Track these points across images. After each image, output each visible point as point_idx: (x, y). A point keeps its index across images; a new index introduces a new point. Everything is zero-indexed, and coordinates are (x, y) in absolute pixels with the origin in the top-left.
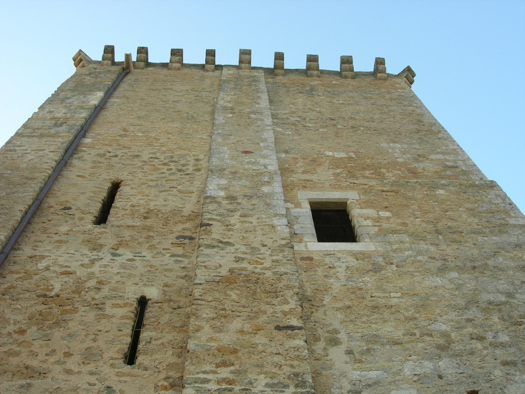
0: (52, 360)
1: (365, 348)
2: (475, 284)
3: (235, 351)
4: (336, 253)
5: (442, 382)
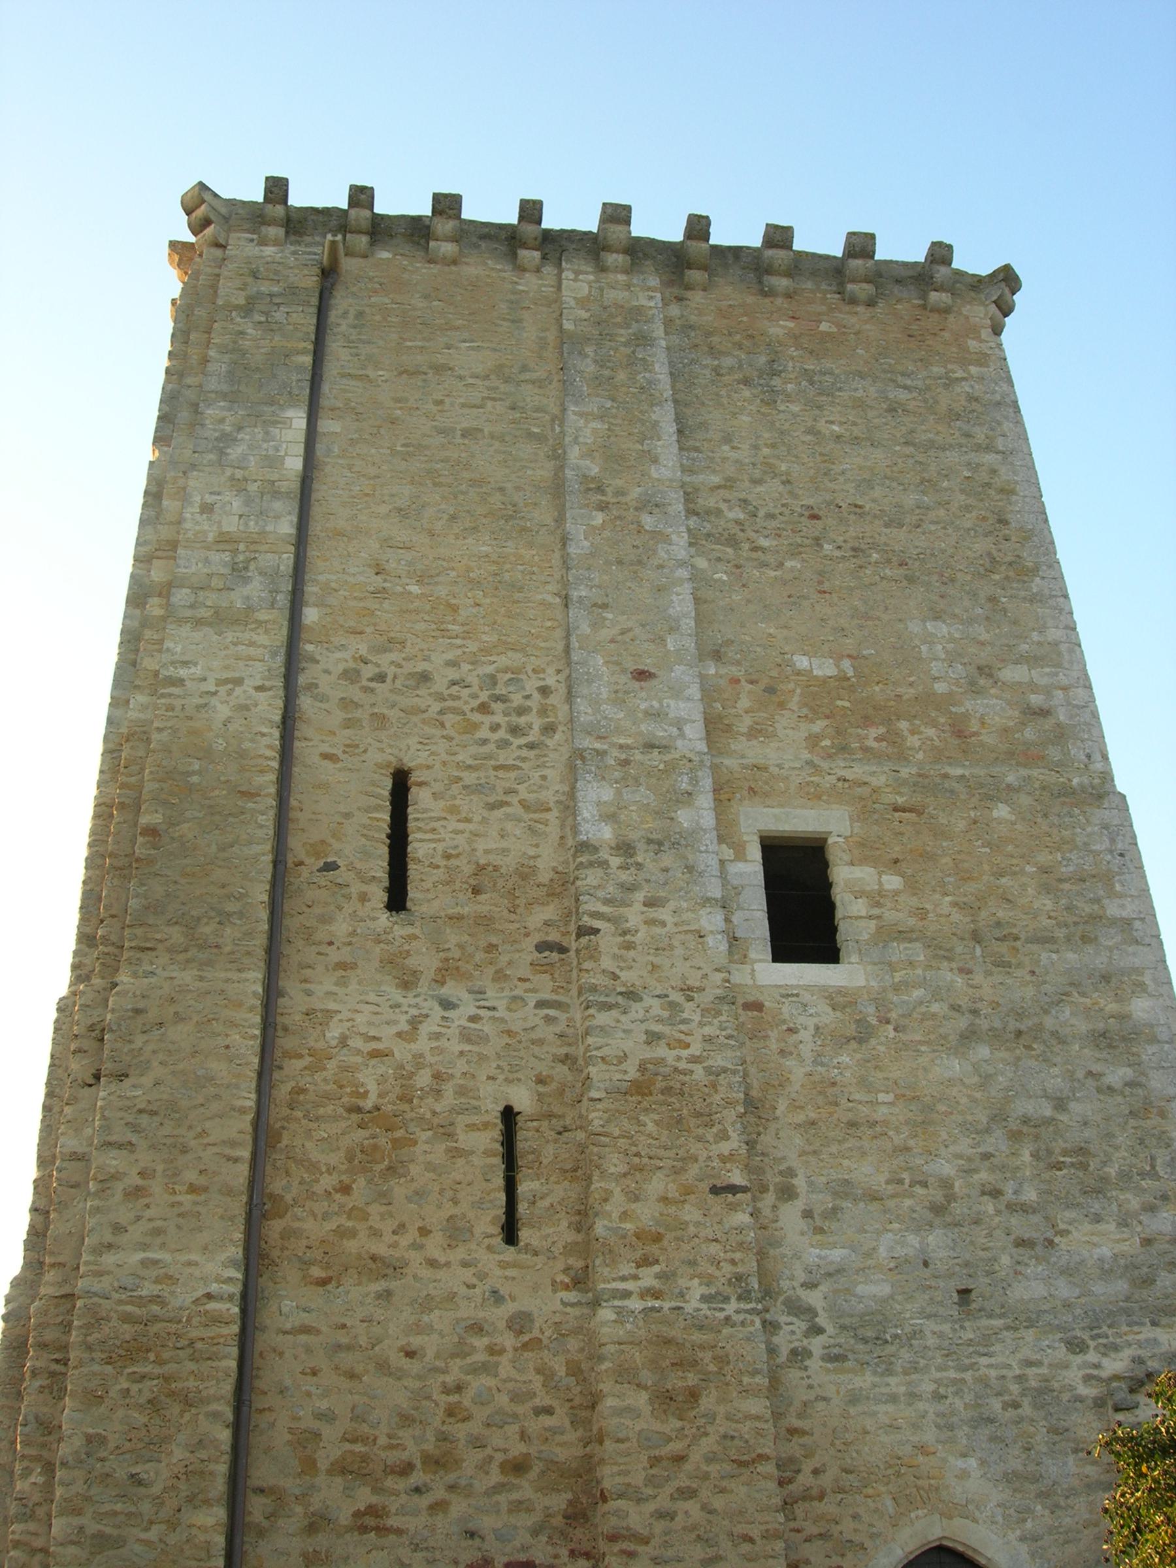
0: (404, 1241)
1: (830, 1206)
2: (1011, 1075)
3: (658, 1238)
4: (802, 992)
5: (927, 1273)
